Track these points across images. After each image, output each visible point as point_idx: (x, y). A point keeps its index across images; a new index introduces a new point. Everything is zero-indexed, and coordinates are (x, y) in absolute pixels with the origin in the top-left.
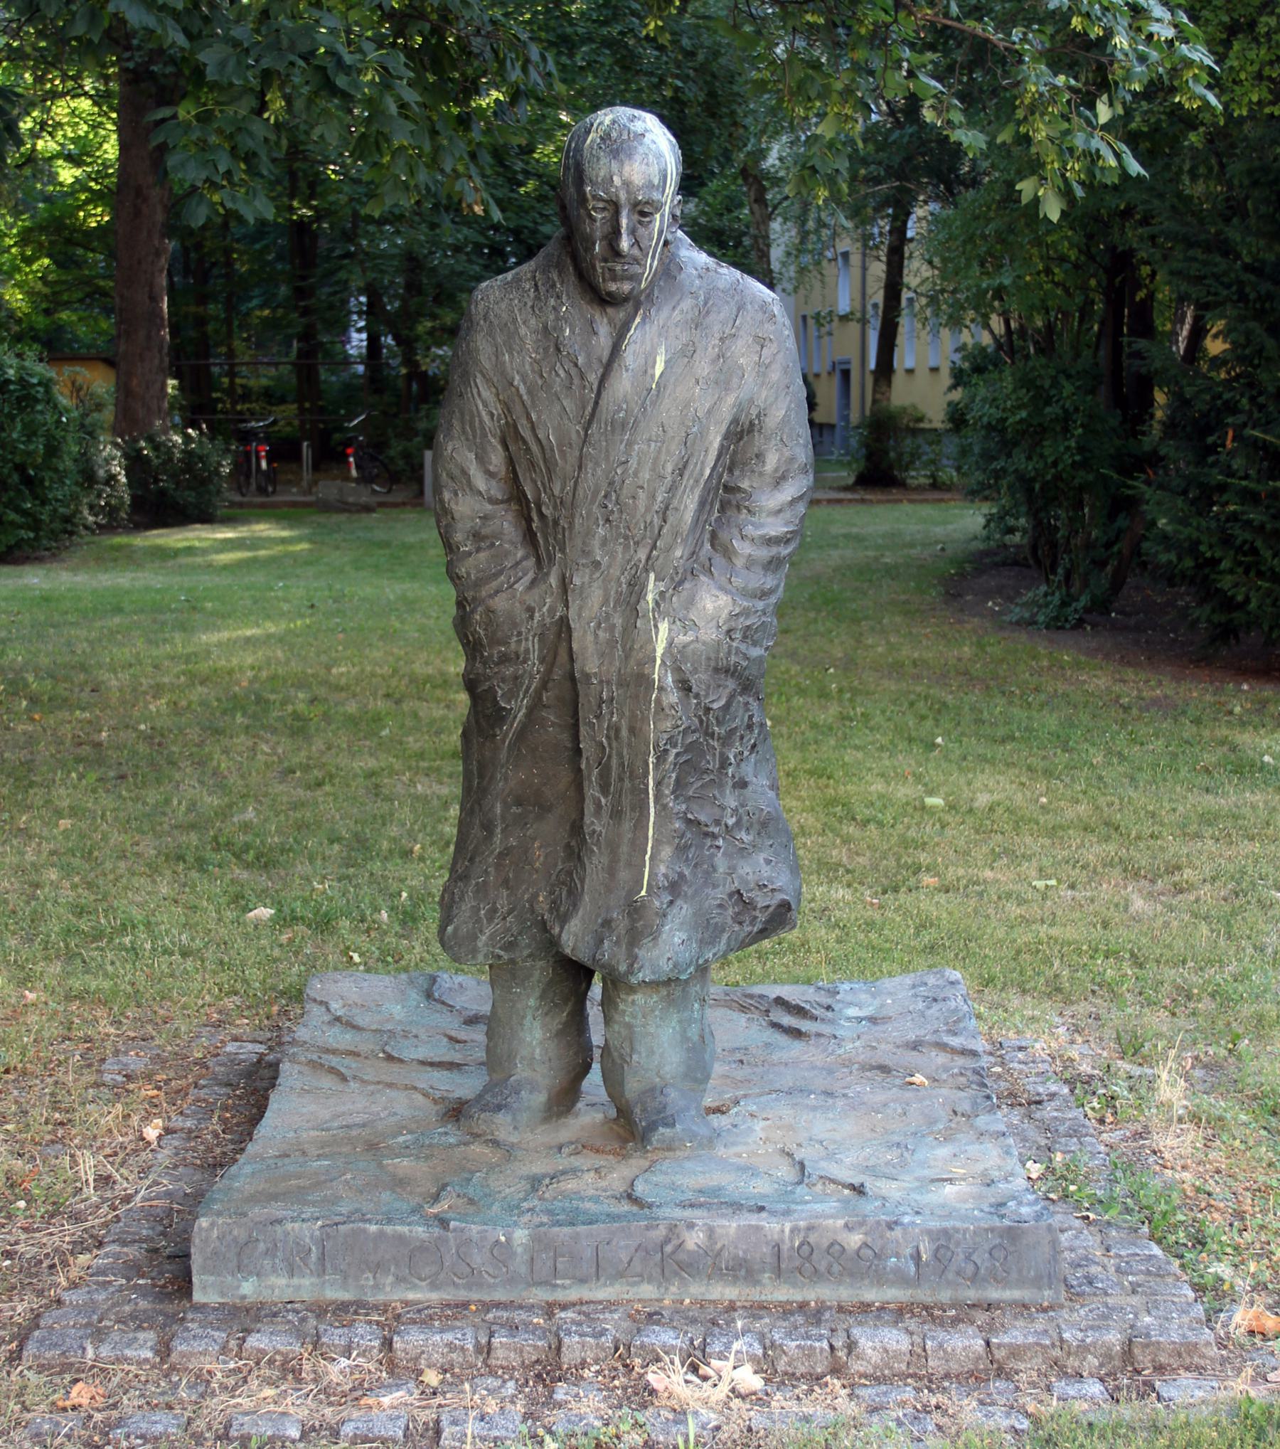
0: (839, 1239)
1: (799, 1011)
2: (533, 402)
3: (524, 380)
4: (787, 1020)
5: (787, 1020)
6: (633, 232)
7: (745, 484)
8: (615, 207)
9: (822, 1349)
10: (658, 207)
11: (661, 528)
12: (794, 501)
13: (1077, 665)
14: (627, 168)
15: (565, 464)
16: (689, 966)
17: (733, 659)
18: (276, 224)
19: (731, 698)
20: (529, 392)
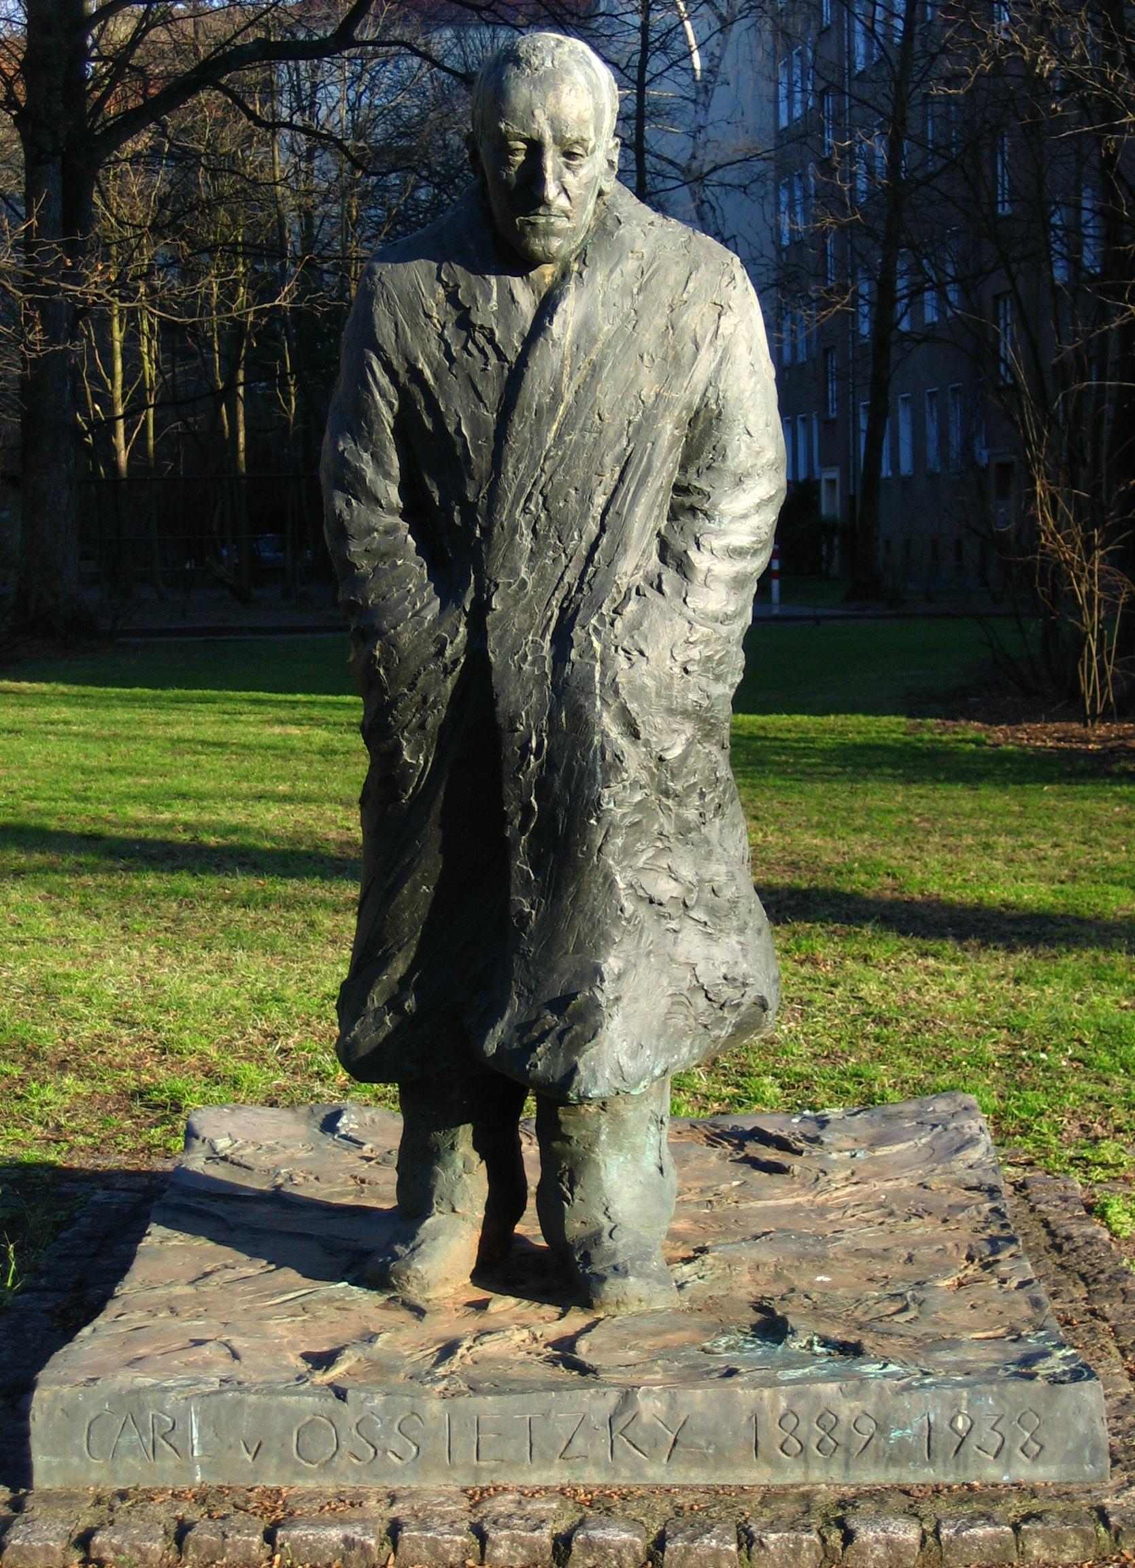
0: (832, 1407)
1: (781, 1144)
2: (441, 387)
3: (430, 365)
4: (769, 1154)
5: (769, 1154)
6: (559, 178)
7: (701, 484)
8: (535, 148)
9: (811, 1543)
10: (589, 152)
11: (599, 537)
12: (759, 506)
13: (1111, 784)
14: (551, 99)
15: (481, 463)
16: (641, 1079)
17: (692, 696)
18: (83, 55)
19: (690, 743)
20: (434, 375)
